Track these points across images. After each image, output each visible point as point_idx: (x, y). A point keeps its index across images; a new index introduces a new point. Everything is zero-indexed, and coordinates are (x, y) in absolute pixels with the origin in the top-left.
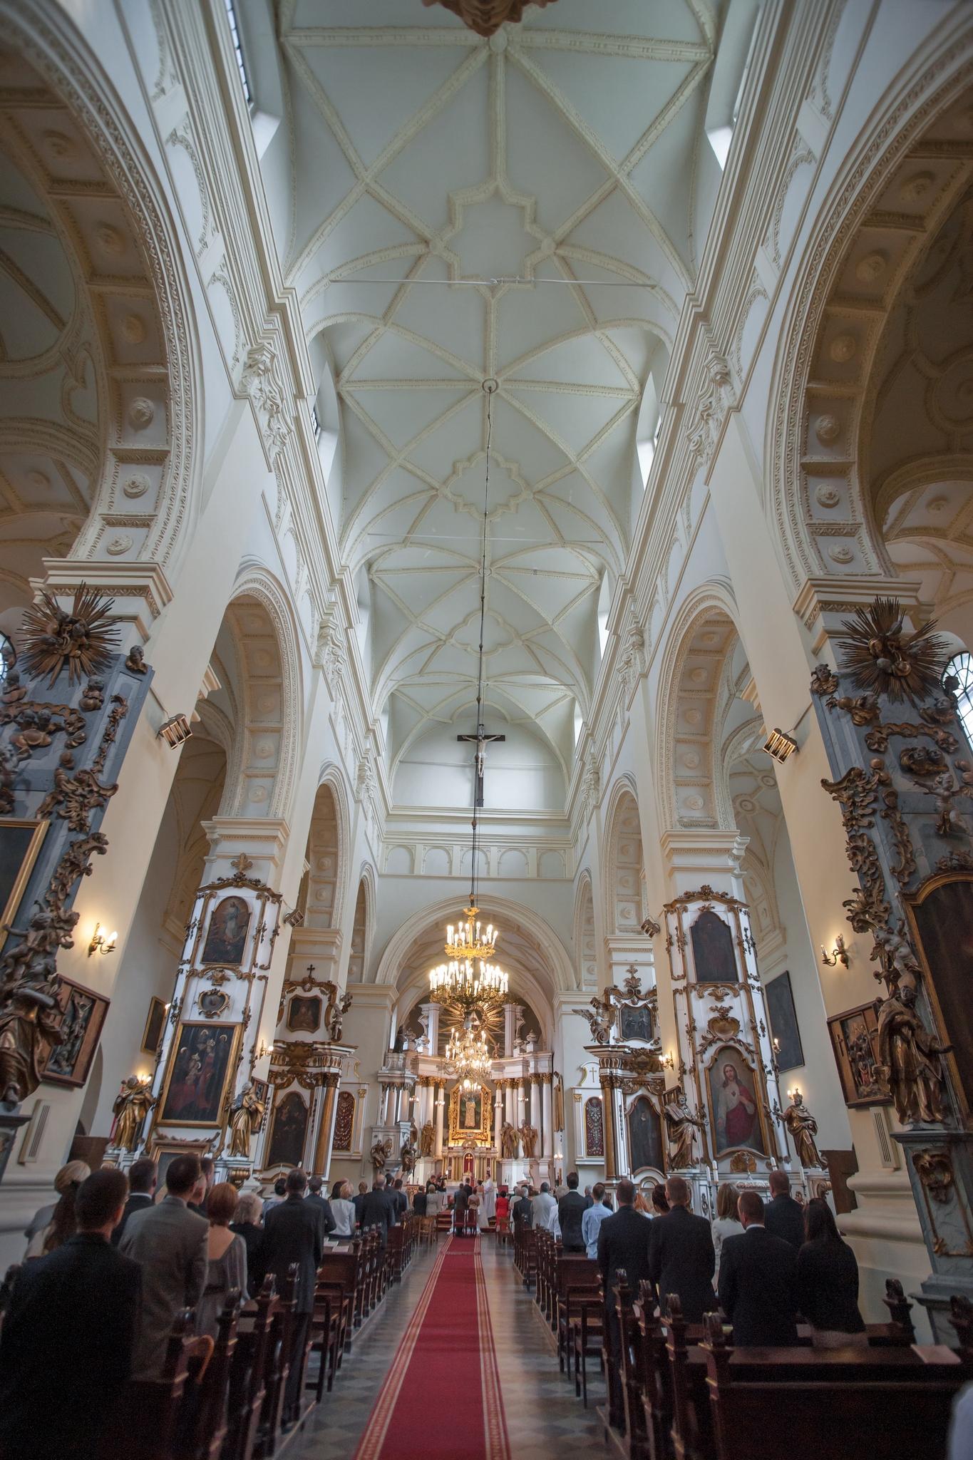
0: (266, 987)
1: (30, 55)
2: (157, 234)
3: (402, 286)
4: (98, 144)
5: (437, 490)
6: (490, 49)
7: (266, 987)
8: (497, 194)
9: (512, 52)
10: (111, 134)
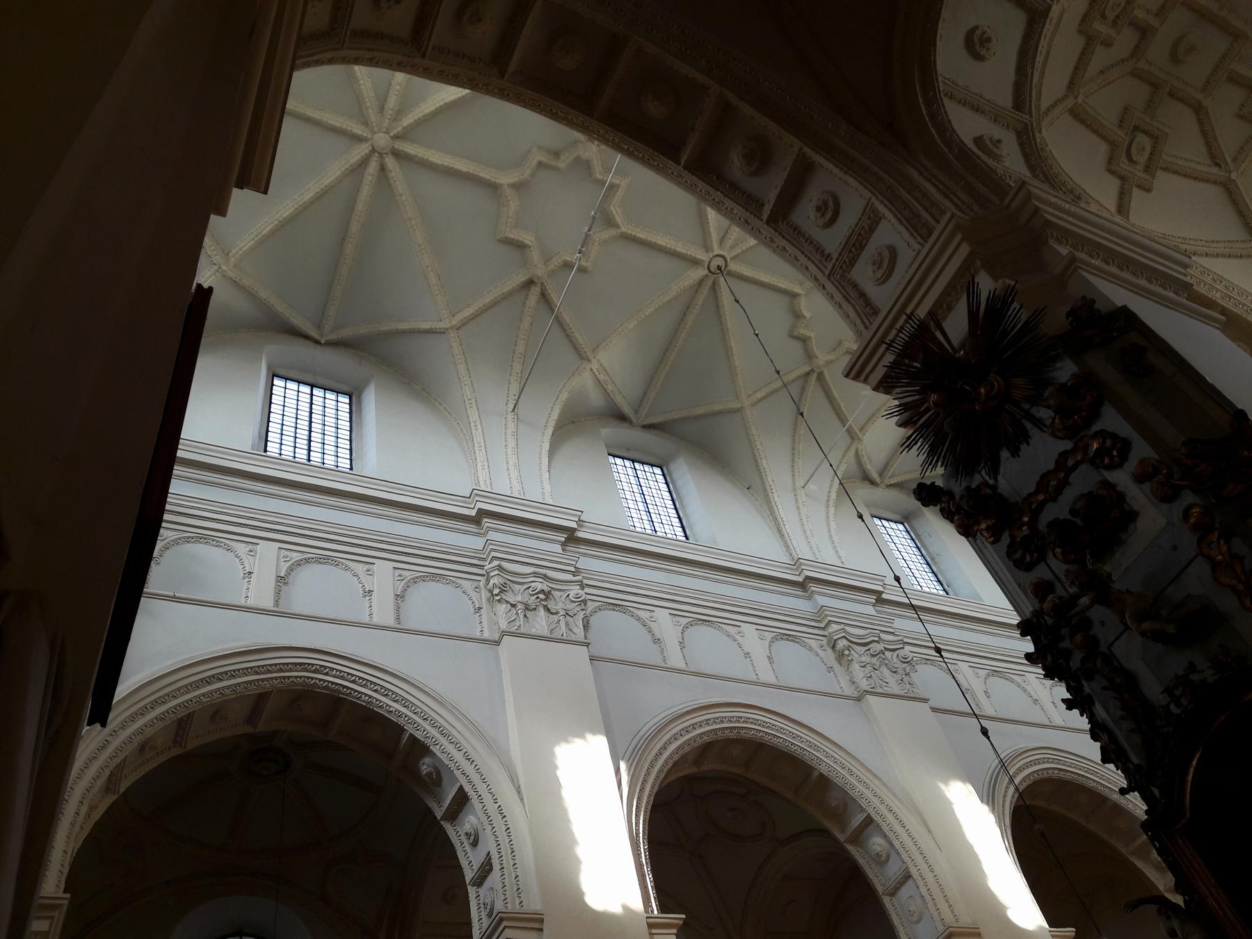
1: (149, 732)
2: (313, 672)
3: (558, 320)
5: (812, 371)
6: (386, 154)
8: (517, 187)
9: (395, 132)
10: (228, 679)
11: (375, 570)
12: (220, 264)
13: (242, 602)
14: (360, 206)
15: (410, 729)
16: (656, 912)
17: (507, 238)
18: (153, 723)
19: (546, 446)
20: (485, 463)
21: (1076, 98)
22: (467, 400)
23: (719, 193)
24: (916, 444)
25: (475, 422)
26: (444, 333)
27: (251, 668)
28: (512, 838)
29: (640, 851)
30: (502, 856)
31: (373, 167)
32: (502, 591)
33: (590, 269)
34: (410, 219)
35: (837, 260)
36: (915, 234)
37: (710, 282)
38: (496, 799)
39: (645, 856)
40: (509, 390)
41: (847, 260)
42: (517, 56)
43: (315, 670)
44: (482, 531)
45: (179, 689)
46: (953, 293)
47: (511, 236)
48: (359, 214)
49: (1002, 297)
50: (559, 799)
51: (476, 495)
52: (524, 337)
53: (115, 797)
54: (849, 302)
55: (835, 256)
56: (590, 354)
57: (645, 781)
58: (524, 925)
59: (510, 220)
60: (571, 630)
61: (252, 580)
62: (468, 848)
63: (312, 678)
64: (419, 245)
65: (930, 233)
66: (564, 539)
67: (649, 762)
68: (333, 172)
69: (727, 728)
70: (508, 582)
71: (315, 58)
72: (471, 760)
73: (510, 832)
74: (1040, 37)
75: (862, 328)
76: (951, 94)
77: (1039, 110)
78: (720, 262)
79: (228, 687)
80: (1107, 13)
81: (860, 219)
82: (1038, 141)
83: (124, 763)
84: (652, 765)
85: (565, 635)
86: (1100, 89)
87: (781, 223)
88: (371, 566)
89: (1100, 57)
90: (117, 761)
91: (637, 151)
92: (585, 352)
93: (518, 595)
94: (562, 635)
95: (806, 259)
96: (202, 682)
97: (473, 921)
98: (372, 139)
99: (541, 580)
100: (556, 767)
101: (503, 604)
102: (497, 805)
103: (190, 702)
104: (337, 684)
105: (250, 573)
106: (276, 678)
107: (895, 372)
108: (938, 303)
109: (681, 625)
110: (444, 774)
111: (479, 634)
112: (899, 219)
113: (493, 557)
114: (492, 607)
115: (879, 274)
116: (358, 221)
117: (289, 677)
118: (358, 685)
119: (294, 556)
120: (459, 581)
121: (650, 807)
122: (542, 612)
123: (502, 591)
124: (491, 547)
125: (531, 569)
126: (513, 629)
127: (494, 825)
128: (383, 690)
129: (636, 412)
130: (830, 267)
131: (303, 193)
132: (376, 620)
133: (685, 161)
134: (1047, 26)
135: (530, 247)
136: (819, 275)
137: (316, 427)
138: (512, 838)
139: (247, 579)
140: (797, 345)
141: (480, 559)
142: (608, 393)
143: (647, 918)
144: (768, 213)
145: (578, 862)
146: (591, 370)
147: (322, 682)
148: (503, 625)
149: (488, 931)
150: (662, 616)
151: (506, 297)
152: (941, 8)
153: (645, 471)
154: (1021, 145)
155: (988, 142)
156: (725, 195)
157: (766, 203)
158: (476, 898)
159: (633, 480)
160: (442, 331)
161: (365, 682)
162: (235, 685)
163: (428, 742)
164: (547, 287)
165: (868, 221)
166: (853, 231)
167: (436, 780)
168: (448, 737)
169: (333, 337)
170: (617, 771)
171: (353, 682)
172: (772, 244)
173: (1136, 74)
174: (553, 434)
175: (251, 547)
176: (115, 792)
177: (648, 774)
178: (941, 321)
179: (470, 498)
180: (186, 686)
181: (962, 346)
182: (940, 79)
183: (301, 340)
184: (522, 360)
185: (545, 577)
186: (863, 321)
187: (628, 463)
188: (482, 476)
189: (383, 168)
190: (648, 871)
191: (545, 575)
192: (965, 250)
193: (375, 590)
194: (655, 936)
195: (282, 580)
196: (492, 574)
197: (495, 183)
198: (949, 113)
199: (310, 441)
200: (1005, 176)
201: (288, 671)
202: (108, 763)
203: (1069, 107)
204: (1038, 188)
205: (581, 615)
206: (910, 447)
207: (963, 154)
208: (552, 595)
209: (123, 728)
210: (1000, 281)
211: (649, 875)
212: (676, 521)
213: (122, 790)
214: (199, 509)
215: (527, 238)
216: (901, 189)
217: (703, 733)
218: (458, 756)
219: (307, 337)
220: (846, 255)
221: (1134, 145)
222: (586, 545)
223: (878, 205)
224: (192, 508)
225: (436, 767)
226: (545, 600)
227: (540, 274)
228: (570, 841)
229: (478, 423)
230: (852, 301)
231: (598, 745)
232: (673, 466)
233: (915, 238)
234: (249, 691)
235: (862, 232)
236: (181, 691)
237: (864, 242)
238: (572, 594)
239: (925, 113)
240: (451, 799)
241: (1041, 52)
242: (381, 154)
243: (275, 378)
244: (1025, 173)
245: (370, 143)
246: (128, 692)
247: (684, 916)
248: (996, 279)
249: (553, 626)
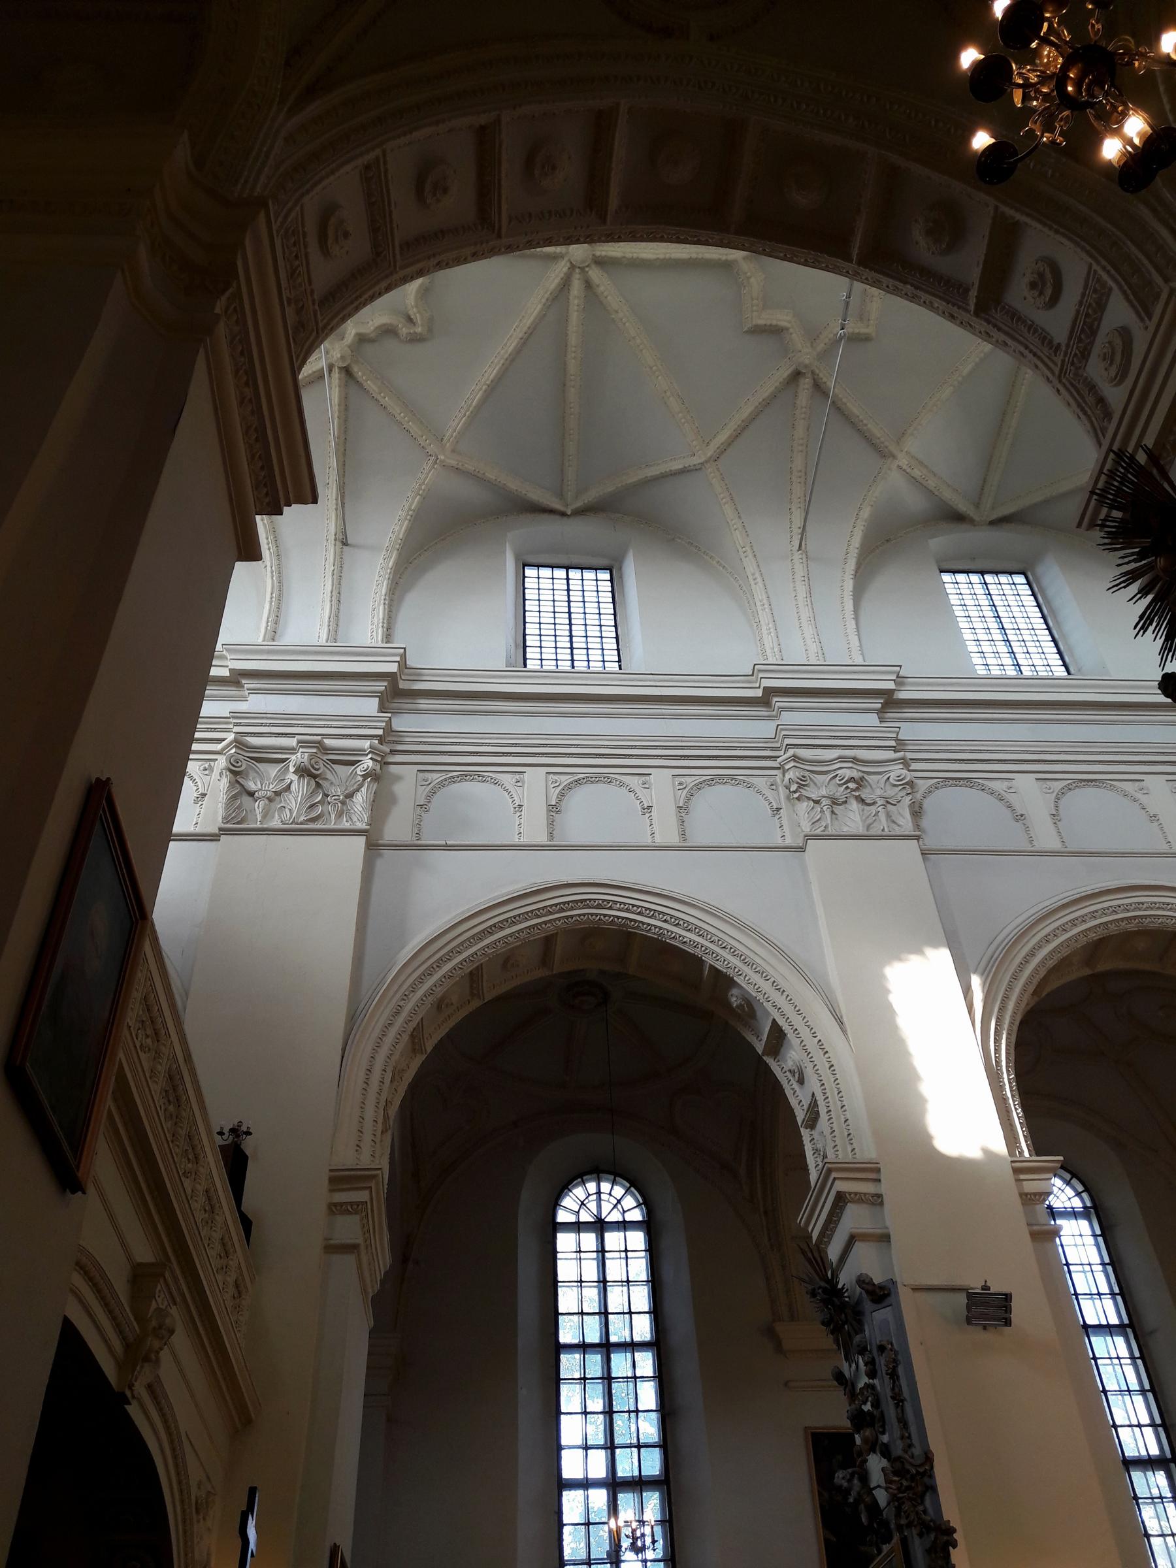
0: (633, 1561)
1: (440, 992)
4: (512, 943)
7: (633, 1561)
11: (652, 781)
12: (436, 455)
13: (516, 840)
14: (573, 339)
15: (709, 960)
16: (1026, 1154)
17: (756, 326)
18: (442, 982)
19: (849, 585)
20: (770, 626)
22: (740, 550)
23: (909, 286)
24: (1151, 624)
25: (753, 574)
26: (700, 469)
27: (532, 911)
28: (837, 1076)
29: (1003, 1082)
30: (828, 1097)
31: (577, 287)
32: (801, 786)
33: (874, 334)
34: (634, 338)
38: (815, 1033)
39: (1011, 1087)
40: (791, 522)
41: (1078, 352)
43: (598, 905)
44: (774, 713)
45: (462, 944)
47: (761, 322)
48: (573, 349)
50: (894, 1029)
51: (760, 671)
52: (800, 448)
53: (424, 1057)
56: (893, 448)
57: (1006, 998)
58: (852, 1175)
59: (755, 302)
60: (894, 822)
61: (523, 813)
62: (796, 1086)
63: (597, 915)
64: (651, 368)
66: (880, 705)
67: (1010, 973)
68: (534, 306)
69: (1122, 919)
70: (807, 774)
72: (781, 990)
73: (834, 1070)
79: (511, 935)
81: (1083, 295)
83: (422, 1024)
84: (1015, 977)
85: (886, 830)
88: (647, 778)
90: (413, 1025)
92: (887, 447)
93: (821, 788)
94: (883, 830)
96: (484, 933)
97: (810, 1167)
98: (567, 253)
99: (850, 765)
100: (888, 991)
101: (803, 801)
102: (816, 1040)
103: (475, 956)
104: (623, 918)
105: (520, 806)
106: (559, 919)
109: (1053, 792)
110: (756, 1007)
111: (780, 841)
113: (787, 745)
114: (793, 805)
115: (1113, 371)
116: (574, 358)
117: (572, 917)
118: (646, 916)
119: (563, 780)
120: (749, 779)
121: (1015, 1028)
122: (854, 805)
123: (801, 786)
124: (784, 733)
125: (835, 753)
126: (818, 832)
127: (815, 1063)
128: (673, 920)
129: (977, 506)
130: (1059, 360)
131: (506, 343)
132: (659, 840)
135: (787, 329)
137: (577, 619)
138: (837, 1076)
139: (518, 814)
141: (773, 749)
142: (931, 491)
143: (1012, 1162)
144: (974, 301)
145: (922, 1101)
146: (900, 467)
147: (607, 918)
148: (806, 828)
149: (820, 1181)
150: (1026, 784)
151: (767, 404)
153: (1001, 584)
156: (917, 288)
158: (811, 1141)
159: (984, 601)
160: (697, 467)
161: (652, 912)
162: (518, 932)
163: (730, 972)
164: (821, 375)
165: (1094, 296)
167: (749, 1011)
168: (752, 966)
169: (579, 504)
170: (967, 991)
171: (639, 914)
174: (856, 572)
175: (517, 777)
176: (422, 1053)
177: (1010, 988)
179: (752, 675)
180: (468, 939)
183: (546, 516)
184: (803, 480)
185: (855, 760)
187: (975, 578)
188: (769, 642)
189: (588, 285)
190: (1015, 1105)
191: (854, 758)
193: (654, 805)
194: (1024, 1183)
195: (554, 809)
196: (787, 767)
197: (726, 260)
199: (571, 636)
201: (569, 910)
202: (404, 1028)
205: (907, 800)
206: (1144, 629)
208: (866, 780)
209: (413, 991)
211: (1016, 1109)
212: (1050, 648)
213: (429, 1049)
214: (459, 744)
215: (781, 318)
216: (1129, 243)
217: (1089, 929)
218: (766, 986)
219: (552, 511)
220: (1075, 347)
222: (910, 708)
224: (452, 744)
225: (746, 998)
226: (857, 789)
227: (807, 362)
228: (912, 1077)
229: (757, 575)
230: (1089, 412)
231: (940, 959)
232: (1040, 569)
234: (534, 935)
235: (1090, 311)
236: (464, 945)
237: (1096, 323)
238: (893, 775)
240: (767, 1032)
242: (582, 269)
243: (526, 567)
245: (566, 259)
246: (418, 948)
247: (1061, 1158)
249: (869, 821)
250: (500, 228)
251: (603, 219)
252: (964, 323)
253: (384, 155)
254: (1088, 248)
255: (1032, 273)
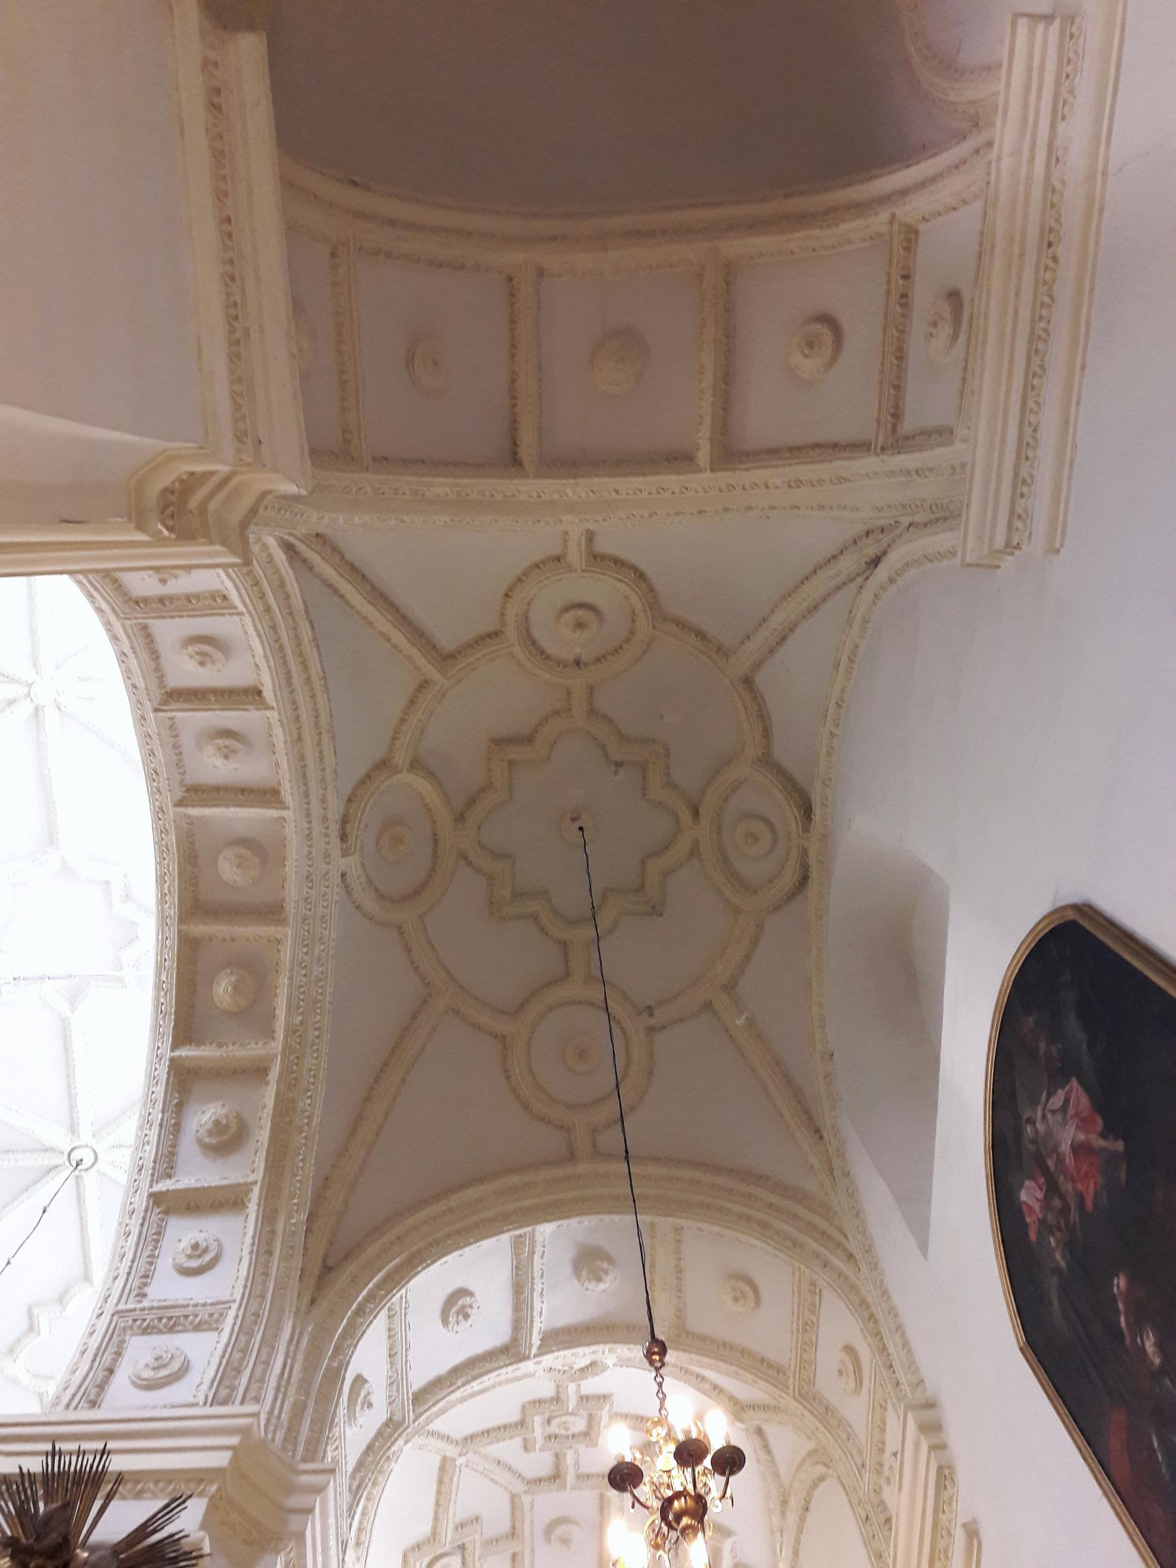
21: (460, 1455)
23: (160, 1116)
35: (143, 1309)
36: (215, 1384)
37: (55, 1160)
42: (207, 812)
46: (161, 1485)
49: (180, 1552)
54: (93, 1361)
55: (146, 1303)
65: (225, 1402)
71: (95, 593)
74: (496, 1369)
75: (66, 1399)
76: (394, 1316)
77: (428, 1425)
78: (88, 1160)
80: (554, 1422)
81: (204, 1305)
82: (393, 1449)
86: (482, 1473)
87: (158, 1211)
89: (509, 1449)
91: (166, 994)
95: (127, 1270)
107: (18, 1487)
108: (139, 1476)
112: (225, 1351)
115: (147, 1374)
130: (130, 1306)
133: (180, 1056)
134: (510, 1369)
136: (113, 1300)
140: (24, 1324)
152: (471, 1244)
154: (379, 1434)
155: (363, 1393)
156: (161, 1125)
157: (173, 1180)
165: (207, 1316)
166: (188, 1306)
172: (127, 1216)
173: (514, 1499)
178: (117, 1496)
181: (93, 1549)
182: (403, 1291)
186: (74, 1396)
192: (221, 1460)
198: (372, 1326)
200: (336, 1440)
203: (447, 1454)
204: (337, 1491)
207: (335, 1375)
210: (202, 1534)
221: (445, 1561)
223: (231, 1314)
230: (96, 1364)
233: (211, 1387)
235: (191, 1318)
239: (360, 1298)
241: (498, 1375)
244: (351, 1467)
248: (203, 1526)
250: (164, 711)
251: (180, 803)
252: (136, 1184)
253: (238, 614)
254: (247, 1291)
255: (205, 1240)
